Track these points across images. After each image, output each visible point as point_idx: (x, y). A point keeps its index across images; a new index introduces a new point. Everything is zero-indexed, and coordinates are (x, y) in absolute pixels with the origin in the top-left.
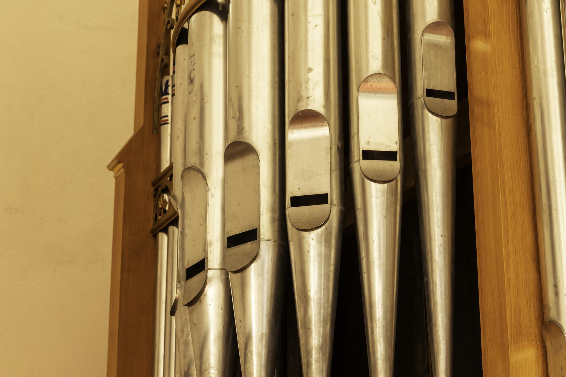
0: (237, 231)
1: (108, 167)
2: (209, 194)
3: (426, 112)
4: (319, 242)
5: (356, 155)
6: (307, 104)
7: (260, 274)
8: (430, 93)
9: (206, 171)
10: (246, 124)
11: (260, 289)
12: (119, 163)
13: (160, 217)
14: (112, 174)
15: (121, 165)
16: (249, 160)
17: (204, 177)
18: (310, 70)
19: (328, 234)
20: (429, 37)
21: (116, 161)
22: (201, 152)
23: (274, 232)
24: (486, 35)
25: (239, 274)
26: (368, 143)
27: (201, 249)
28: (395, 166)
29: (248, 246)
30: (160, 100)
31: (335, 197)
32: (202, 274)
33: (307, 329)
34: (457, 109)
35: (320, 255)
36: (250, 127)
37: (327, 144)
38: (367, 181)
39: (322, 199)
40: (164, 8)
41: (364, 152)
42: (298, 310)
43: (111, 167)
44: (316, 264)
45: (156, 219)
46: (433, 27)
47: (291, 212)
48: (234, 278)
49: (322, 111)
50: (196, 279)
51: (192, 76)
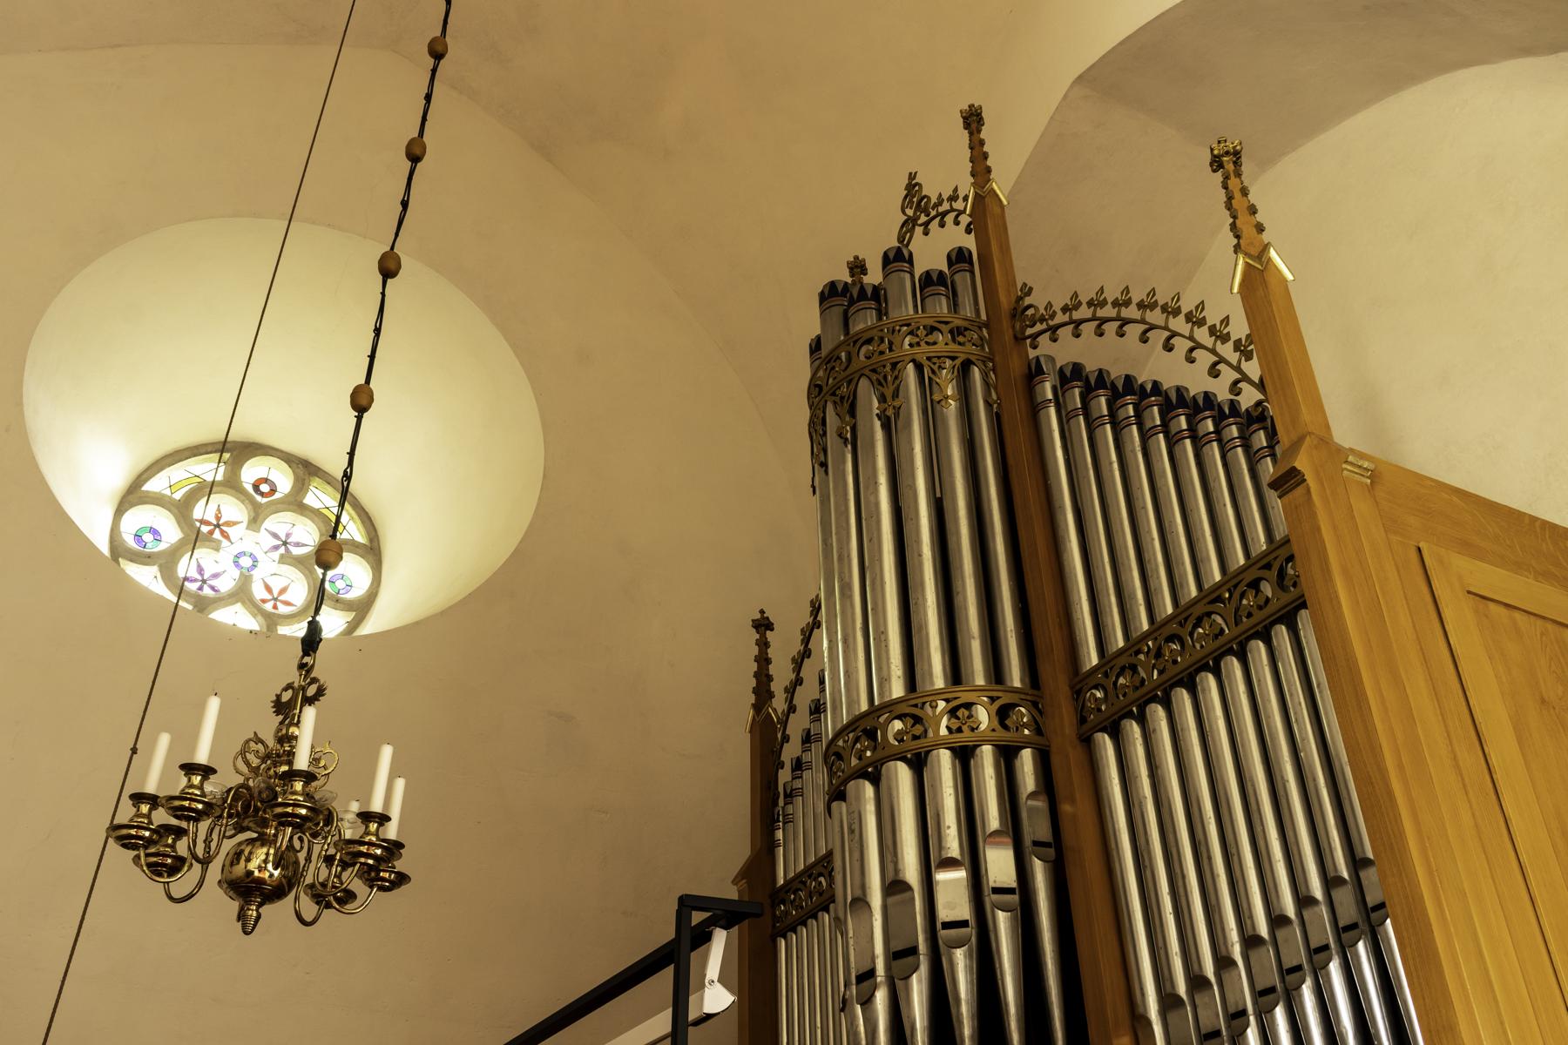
0: (900, 948)
1: (732, 882)
2: (874, 919)
3: (1033, 857)
4: (965, 957)
5: (986, 891)
6: (947, 854)
7: (920, 981)
8: (1036, 843)
9: (868, 899)
10: (900, 867)
11: (920, 992)
12: (742, 879)
13: (778, 925)
14: (735, 887)
15: (744, 881)
16: (907, 895)
17: (869, 907)
18: (949, 827)
19: (970, 950)
20: (1029, 802)
21: (740, 878)
22: (864, 887)
23: (927, 948)
24: (1073, 801)
25: (903, 981)
26: (995, 882)
27: (869, 961)
28: (1015, 898)
29: (910, 959)
30: (773, 827)
31: (972, 923)
32: (871, 981)
33: (961, 1023)
34: (248, 462)
35: (966, 966)
36: (904, 869)
37: (965, 883)
38: (996, 910)
39: (964, 924)
40: (773, 752)
41: (993, 888)
42: (952, 1009)
43: (735, 882)
44: (963, 973)
45: (774, 926)
46: (1032, 795)
47: (943, 934)
48: (899, 984)
49: (959, 857)
50: (866, 984)
51: (853, 827)
